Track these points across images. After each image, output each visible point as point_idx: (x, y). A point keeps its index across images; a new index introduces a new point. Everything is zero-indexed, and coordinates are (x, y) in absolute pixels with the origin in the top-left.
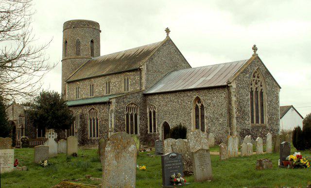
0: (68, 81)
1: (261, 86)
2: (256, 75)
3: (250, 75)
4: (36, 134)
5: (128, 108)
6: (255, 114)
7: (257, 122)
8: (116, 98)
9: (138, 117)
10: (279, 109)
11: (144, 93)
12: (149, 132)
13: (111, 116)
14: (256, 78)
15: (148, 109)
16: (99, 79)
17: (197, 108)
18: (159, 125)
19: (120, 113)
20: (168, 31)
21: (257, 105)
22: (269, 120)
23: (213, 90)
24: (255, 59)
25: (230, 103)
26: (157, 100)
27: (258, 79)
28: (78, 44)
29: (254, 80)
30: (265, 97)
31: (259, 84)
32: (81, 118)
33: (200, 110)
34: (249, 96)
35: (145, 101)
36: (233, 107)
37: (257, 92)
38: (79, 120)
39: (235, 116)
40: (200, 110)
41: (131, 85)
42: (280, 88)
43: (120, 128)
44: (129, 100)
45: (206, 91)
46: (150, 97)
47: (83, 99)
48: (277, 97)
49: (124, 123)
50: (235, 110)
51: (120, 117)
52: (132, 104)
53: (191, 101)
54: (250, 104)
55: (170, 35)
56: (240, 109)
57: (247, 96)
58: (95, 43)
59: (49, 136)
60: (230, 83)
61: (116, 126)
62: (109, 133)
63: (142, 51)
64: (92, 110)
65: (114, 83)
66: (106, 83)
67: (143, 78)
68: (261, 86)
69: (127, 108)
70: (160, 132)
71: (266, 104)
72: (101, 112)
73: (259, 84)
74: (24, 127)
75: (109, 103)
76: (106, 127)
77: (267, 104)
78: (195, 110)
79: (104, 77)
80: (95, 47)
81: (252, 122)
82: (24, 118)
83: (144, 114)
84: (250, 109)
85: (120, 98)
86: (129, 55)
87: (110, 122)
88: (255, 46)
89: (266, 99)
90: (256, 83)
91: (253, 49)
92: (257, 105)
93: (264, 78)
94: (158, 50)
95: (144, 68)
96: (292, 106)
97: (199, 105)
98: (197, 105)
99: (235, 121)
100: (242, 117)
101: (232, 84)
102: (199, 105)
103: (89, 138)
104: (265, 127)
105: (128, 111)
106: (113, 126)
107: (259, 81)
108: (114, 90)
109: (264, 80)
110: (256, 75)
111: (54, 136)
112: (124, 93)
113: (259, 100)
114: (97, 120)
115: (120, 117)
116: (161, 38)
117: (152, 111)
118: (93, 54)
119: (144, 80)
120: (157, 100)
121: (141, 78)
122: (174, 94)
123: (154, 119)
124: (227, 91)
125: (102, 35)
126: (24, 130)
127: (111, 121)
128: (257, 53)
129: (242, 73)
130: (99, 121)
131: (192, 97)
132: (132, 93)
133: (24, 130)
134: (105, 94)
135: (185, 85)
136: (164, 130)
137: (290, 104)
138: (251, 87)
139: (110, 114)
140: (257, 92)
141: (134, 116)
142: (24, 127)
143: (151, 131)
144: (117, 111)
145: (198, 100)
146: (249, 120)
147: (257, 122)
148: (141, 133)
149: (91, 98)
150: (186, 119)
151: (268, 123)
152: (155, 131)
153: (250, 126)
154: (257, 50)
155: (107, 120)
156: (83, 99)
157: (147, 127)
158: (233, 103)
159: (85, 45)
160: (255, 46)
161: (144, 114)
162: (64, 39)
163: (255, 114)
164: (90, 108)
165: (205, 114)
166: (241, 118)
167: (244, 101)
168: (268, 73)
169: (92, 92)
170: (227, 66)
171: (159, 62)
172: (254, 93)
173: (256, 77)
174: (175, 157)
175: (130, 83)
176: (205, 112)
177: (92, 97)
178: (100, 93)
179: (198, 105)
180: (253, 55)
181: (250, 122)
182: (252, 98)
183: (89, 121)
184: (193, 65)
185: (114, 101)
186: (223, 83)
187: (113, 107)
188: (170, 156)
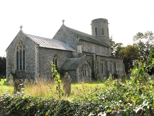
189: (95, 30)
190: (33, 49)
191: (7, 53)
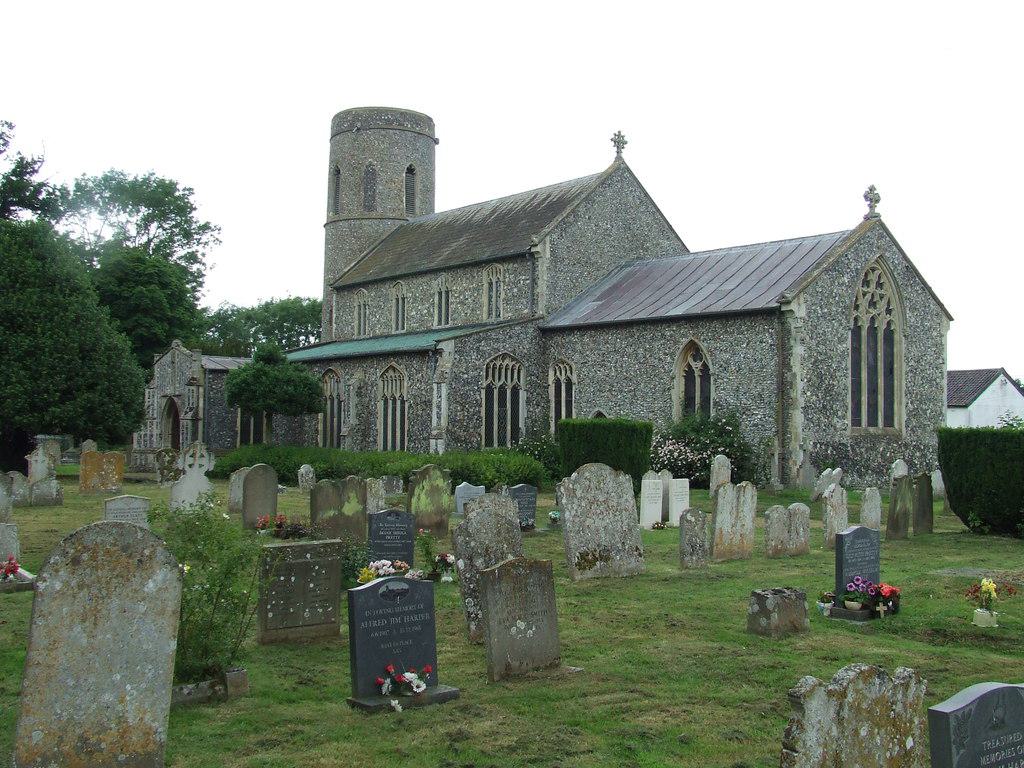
0: (340, 283)
1: (889, 311)
2: (873, 277)
3: (852, 280)
4: (234, 437)
5: (492, 370)
6: (864, 399)
7: (873, 422)
8: (455, 338)
9: (523, 395)
10: (945, 382)
11: (541, 323)
13: (439, 390)
15: (551, 373)
16: (420, 280)
17: (689, 375)
20: (619, 142)
21: (873, 371)
22: (913, 414)
23: (739, 322)
24: (872, 229)
25: (785, 364)
26: (579, 347)
27: (879, 291)
28: (370, 176)
29: (864, 295)
30: (901, 346)
31: (882, 305)
32: (359, 394)
33: (698, 381)
34: (848, 344)
35: (544, 350)
36: (794, 375)
37: (873, 330)
38: (354, 400)
39: (801, 402)
40: (698, 381)
41: (507, 301)
42: (951, 319)
45: (716, 324)
46: (558, 339)
47: (376, 338)
48: (940, 349)
50: (800, 385)
51: (465, 396)
52: (504, 356)
53: (672, 355)
54: (849, 366)
55: (625, 154)
56: (820, 381)
57: (841, 341)
58: (417, 178)
59: (190, 460)
60: (789, 303)
61: (452, 421)
62: (433, 442)
64: (391, 373)
65: (461, 293)
66: (440, 294)
67: (540, 282)
68: (889, 311)
69: (487, 368)
71: (901, 368)
72: (406, 383)
73: (882, 305)
75: (429, 354)
76: (426, 423)
77: (905, 368)
78: (683, 381)
80: (419, 187)
81: (856, 422)
82: (201, 390)
84: (849, 382)
85: (471, 334)
86: (510, 210)
87: (435, 410)
88: (872, 189)
89: (904, 351)
90: (873, 304)
91: (866, 197)
92: (873, 371)
93: (898, 286)
94: (586, 199)
95: (544, 251)
96: (1003, 371)
97: (697, 366)
98: (689, 366)
99: (798, 418)
100: (824, 407)
101: (793, 306)
102: (697, 366)
104: (897, 437)
105: (490, 378)
106: (444, 422)
107: (882, 297)
108: (460, 315)
109: (899, 293)
110: (873, 277)
111: (205, 461)
112: (485, 325)
113: (880, 354)
114: (403, 402)
115: (465, 396)
116: (600, 161)
117: (563, 378)
118: (413, 209)
119: (542, 288)
120: (579, 347)
121: (534, 281)
122: (625, 332)
124: (776, 325)
125: (441, 153)
126: (200, 424)
127: (439, 407)
128: (877, 210)
129: (826, 270)
131: (676, 342)
132: (509, 324)
133: (200, 424)
134: (435, 326)
135: (660, 304)
137: (997, 366)
138: (855, 314)
139: (435, 386)
140: (873, 330)
141: (496, 392)
142: (201, 415)
144: (456, 378)
145: (693, 349)
147: (873, 422)
149: (397, 335)
150: (657, 405)
151: (907, 426)
153: (848, 432)
154: (877, 201)
155: (428, 403)
156: (376, 338)
158: (797, 368)
159: (389, 186)
160: (872, 189)
162: (331, 162)
163: (864, 399)
164: (384, 365)
165: (713, 395)
166: (823, 408)
168: (911, 271)
169: (401, 316)
170: (809, 245)
172: (864, 333)
173: (873, 286)
174: (402, 593)
175: (503, 296)
176: (713, 388)
177: (443, 326)
178: (421, 321)
179: (693, 364)
180: (867, 218)
181: (848, 421)
182: (856, 350)
183: (380, 405)
184: (693, 246)
185: (448, 347)
186: (767, 301)
187: (446, 362)
188: (383, 589)
189: (404, 175)
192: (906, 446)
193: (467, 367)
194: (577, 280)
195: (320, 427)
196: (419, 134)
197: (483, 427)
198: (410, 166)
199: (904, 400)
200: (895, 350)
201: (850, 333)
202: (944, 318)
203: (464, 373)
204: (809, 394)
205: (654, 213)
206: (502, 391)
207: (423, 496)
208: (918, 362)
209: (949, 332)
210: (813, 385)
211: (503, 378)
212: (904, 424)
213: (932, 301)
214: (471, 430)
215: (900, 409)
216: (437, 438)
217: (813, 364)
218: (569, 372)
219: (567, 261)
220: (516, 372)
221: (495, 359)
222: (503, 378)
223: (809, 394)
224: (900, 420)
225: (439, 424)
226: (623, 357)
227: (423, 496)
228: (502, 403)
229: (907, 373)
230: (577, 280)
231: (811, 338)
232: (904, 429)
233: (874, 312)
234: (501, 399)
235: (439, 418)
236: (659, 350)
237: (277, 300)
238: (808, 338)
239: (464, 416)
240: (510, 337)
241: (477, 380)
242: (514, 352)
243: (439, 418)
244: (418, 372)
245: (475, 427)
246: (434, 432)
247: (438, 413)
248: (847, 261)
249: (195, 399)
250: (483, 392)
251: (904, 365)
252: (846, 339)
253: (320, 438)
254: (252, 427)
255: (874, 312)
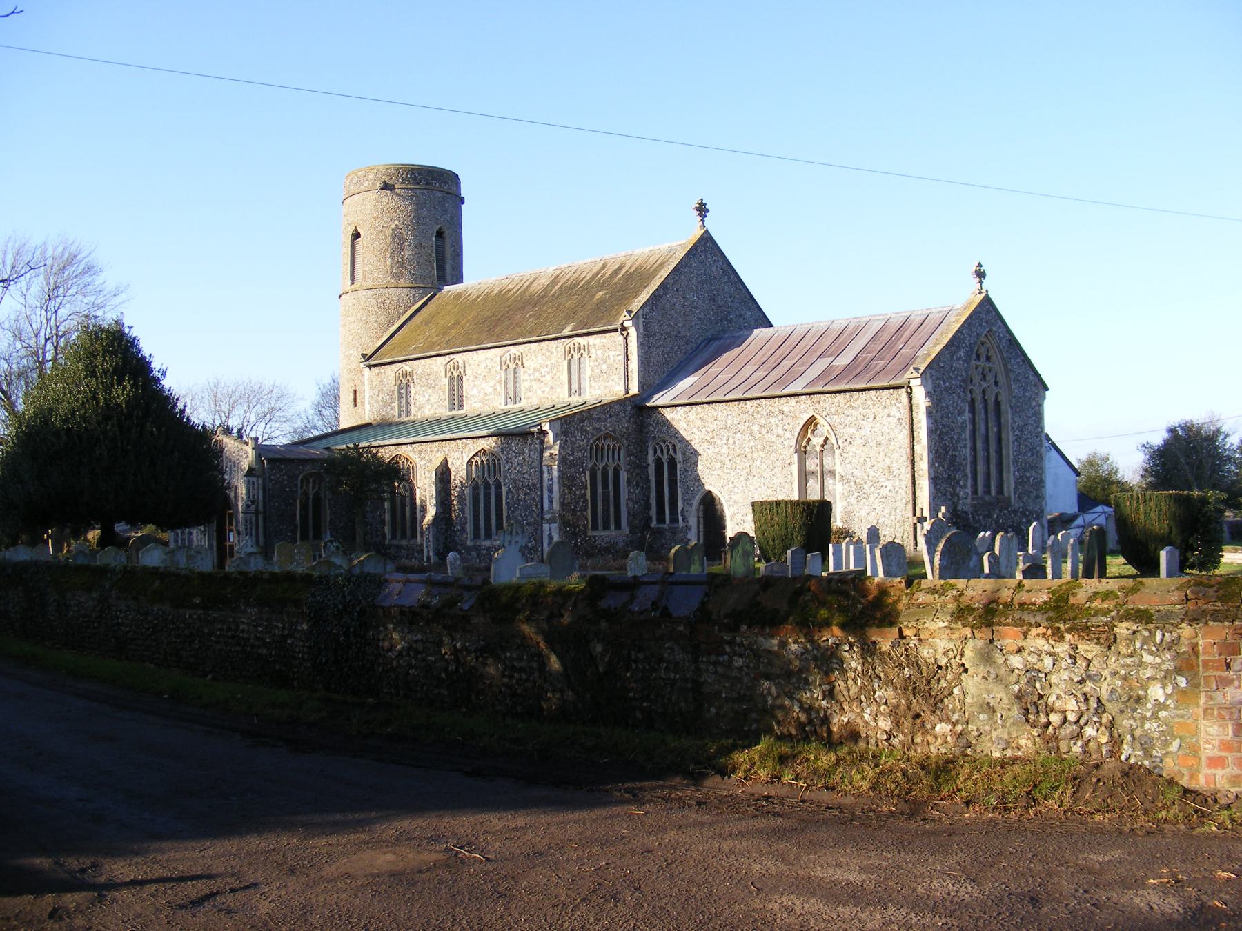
1: (996, 383)
2: (982, 351)
3: (968, 355)
5: (596, 451)
9: (624, 476)
12: (654, 524)
14: (982, 362)
15: (651, 452)
18: (687, 502)
19: (573, 465)
22: (1020, 482)
30: (1008, 417)
34: (967, 416)
42: (1047, 389)
43: (574, 510)
44: (597, 425)
49: (585, 494)
51: (572, 478)
54: (968, 437)
57: (961, 413)
61: (562, 505)
62: (546, 527)
63: (620, 268)
65: (536, 370)
68: (996, 383)
69: (592, 448)
70: (693, 521)
71: (1009, 437)
74: (261, 508)
77: (1011, 438)
79: (875, 392)
80: (449, 251)
83: (639, 467)
84: (968, 452)
88: (980, 265)
103: (469, 543)
106: (556, 506)
109: (1005, 365)
111: (518, 538)
115: (572, 478)
117: (665, 458)
123: (673, 483)
127: (551, 491)
130: (504, 490)
136: (705, 518)
143: (661, 520)
146: (965, 486)
148: (629, 524)
151: (1015, 493)
152: (674, 520)
157: (648, 506)
161: (639, 467)
167: (952, 430)
168: (1013, 343)
171: (678, 307)
173: (983, 358)
189: (434, 239)
190: (1034, 403)
191: (930, 389)
192: (1015, 512)
193: (573, 448)
194: (668, 355)
195: (387, 517)
196: (447, 193)
197: (589, 510)
198: (440, 229)
199: (1012, 469)
200: (1002, 420)
201: (967, 404)
202: (1041, 389)
203: (569, 455)
204: (937, 465)
205: (736, 283)
206: (605, 469)
207: (738, 559)
208: (1022, 431)
209: (1045, 401)
210: (940, 457)
211: (605, 458)
212: (1012, 490)
213: (1031, 372)
214: (578, 514)
215: (1008, 478)
216: (551, 522)
217: (940, 435)
218: (671, 452)
219: (658, 335)
220: (616, 452)
221: (598, 439)
222: (605, 458)
223: (937, 465)
224: (1009, 487)
225: (551, 507)
226: (735, 433)
227: (738, 559)
228: (605, 486)
229: (1013, 442)
230: (668, 355)
231: (937, 411)
232: (1013, 498)
233: (985, 385)
234: (606, 481)
235: (551, 502)
236: (777, 426)
237: (166, 383)
238: (934, 412)
239: (572, 499)
240: (611, 416)
241: (581, 461)
242: (614, 431)
243: (551, 502)
244: (518, 455)
245: (582, 510)
246: (547, 517)
247: (549, 497)
248: (962, 337)
249: (256, 492)
250: (588, 473)
251: (1011, 434)
252: (964, 411)
253: (387, 530)
254: (311, 521)
255: (985, 385)
